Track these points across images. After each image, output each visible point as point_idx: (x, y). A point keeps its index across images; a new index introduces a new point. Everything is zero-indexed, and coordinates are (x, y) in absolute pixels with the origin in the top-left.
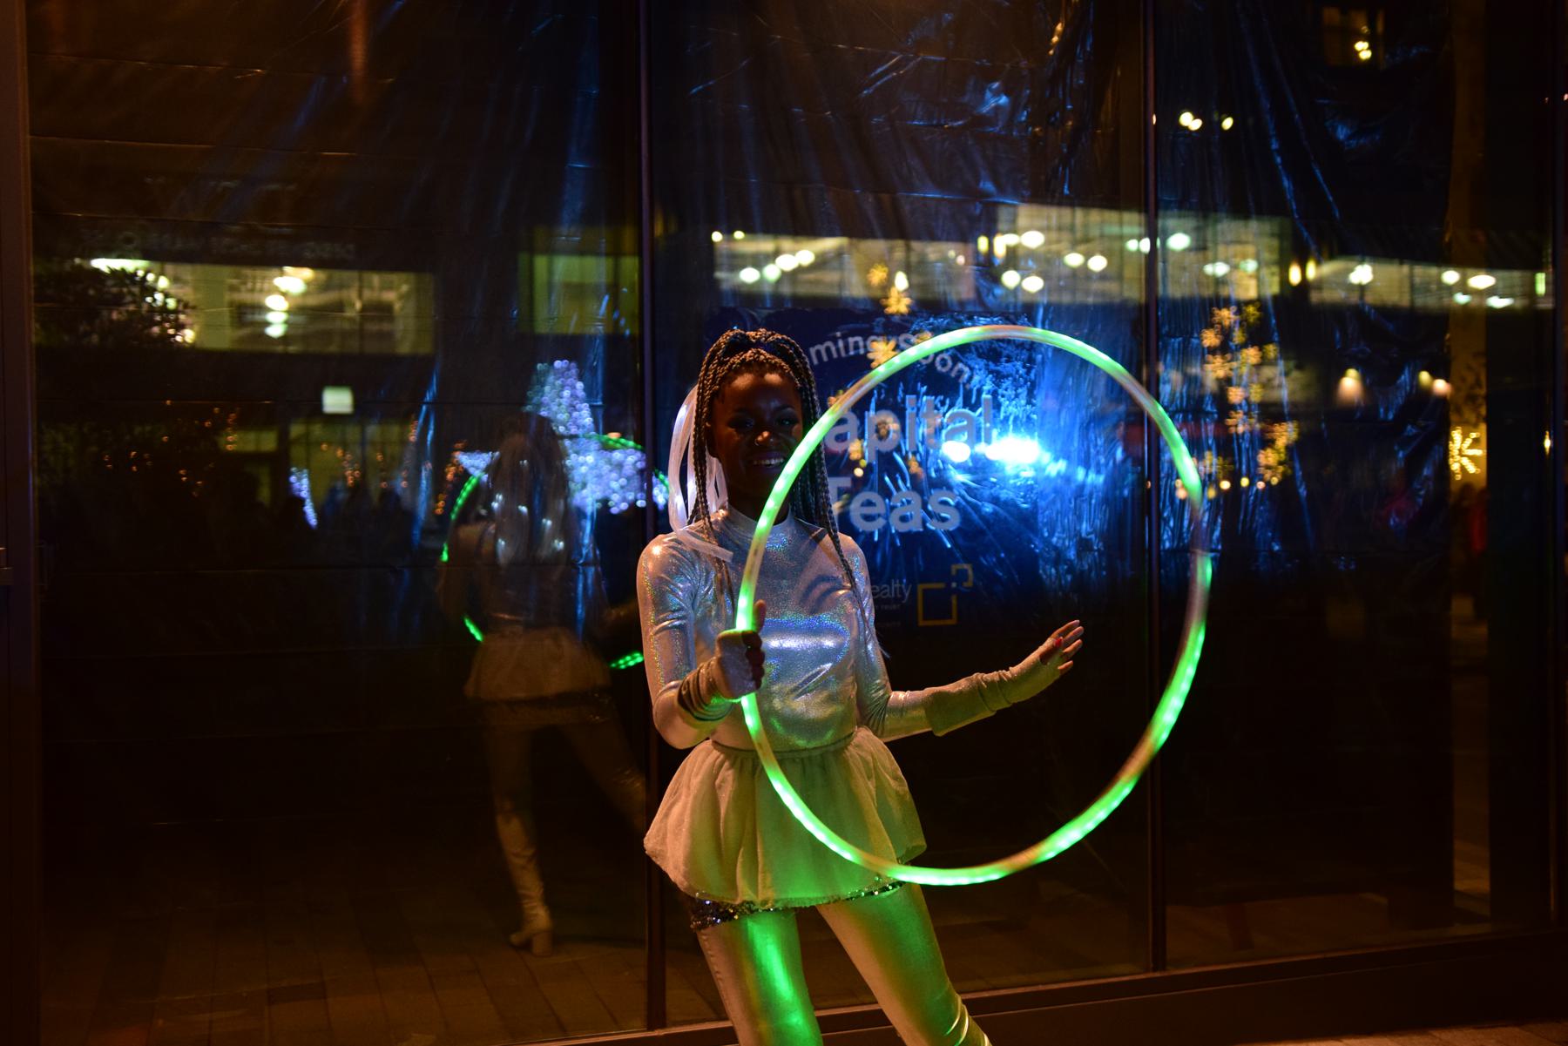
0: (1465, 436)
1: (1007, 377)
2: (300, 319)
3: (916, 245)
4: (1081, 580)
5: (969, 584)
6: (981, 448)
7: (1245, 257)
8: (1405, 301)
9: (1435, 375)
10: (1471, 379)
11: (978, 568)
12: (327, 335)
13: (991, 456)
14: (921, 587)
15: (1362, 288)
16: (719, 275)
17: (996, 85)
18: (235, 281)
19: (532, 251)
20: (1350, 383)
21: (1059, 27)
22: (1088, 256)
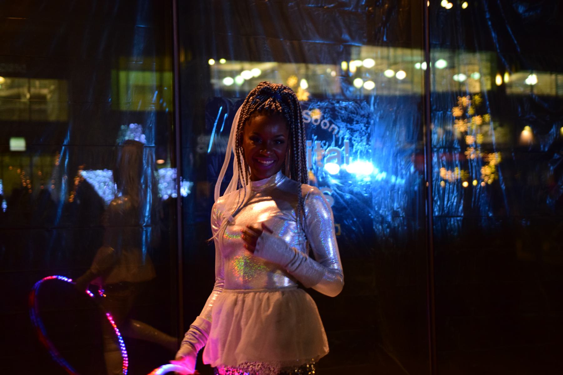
1: (356, 131)
4: (394, 231)
6: (345, 167)
7: (473, 71)
8: (553, 92)
15: (532, 87)
19: (118, 69)
20: (526, 133)
22: (396, 71)
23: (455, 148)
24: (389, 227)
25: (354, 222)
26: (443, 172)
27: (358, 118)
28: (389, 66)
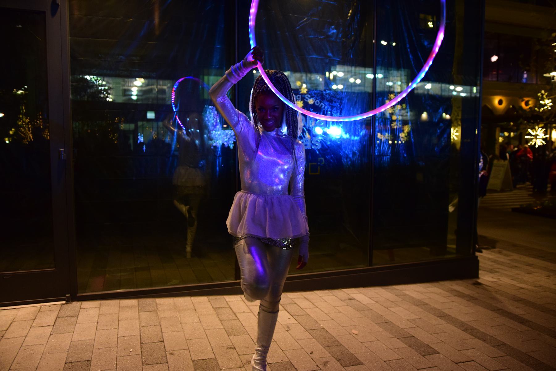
0: (454, 129)
2: (141, 94)
3: (309, 75)
4: (353, 163)
5: (323, 163)
6: (326, 130)
7: (397, 81)
8: (439, 93)
9: (446, 114)
10: (456, 114)
11: (325, 159)
12: (147, 99)
14: (310, 164)
15: (428, 90)
18: (123, 83)
19: (204, 75)
20: (424, 116)
21: (351, 11)
22: (356, 79)
24: (350, 160)
25: (332, 158)
26: (379, 135)
27: (335, 100)
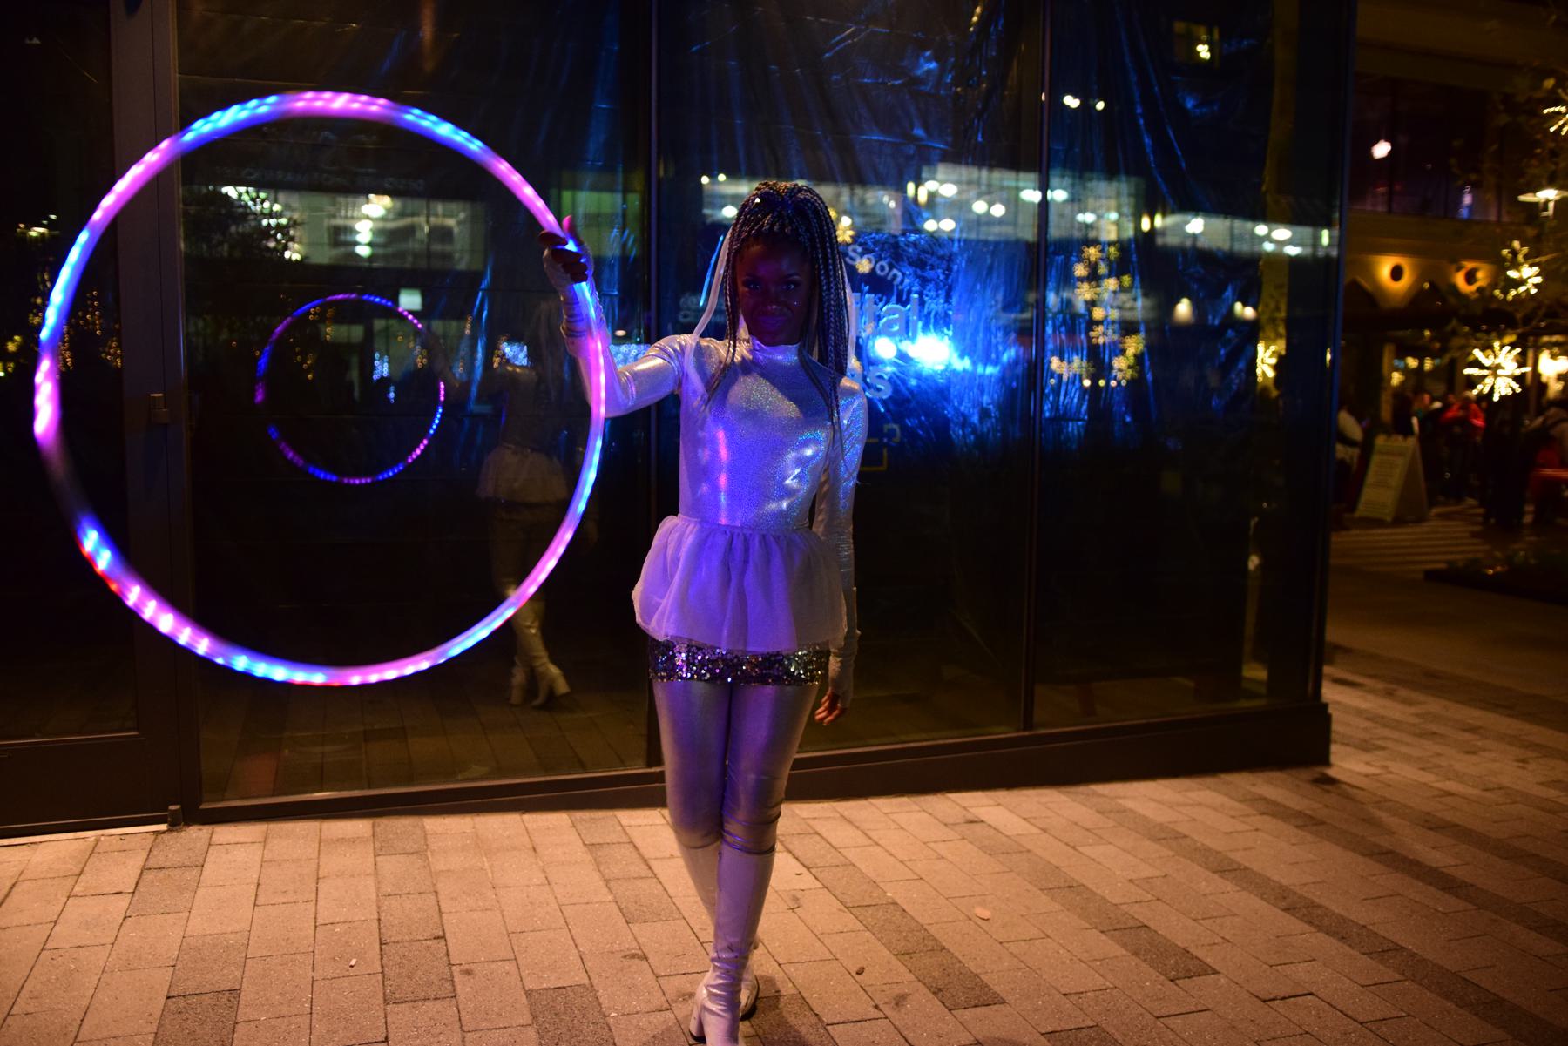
0: (1267, 348)
1: (930, 281)
2: (381, 240)
4: (981, 439)
5: (897, 439)
6: (908, 347)
7: (1108, 210)
8: (1226, 246)
9: (1245, 305)
10: (1272, 305)
11: (904, 428)
12: (401, 255)
13: (911, 354)
15: (1194, 237)
16: (707, 211)
17: (928, 53)
18: (331, 209)
20: (1183, 309)
21: (978, 10)
22: (991, 204)
23: (1077, 323)
26: (1055, 363)
27: (934, 260)
28: (979, 196)
